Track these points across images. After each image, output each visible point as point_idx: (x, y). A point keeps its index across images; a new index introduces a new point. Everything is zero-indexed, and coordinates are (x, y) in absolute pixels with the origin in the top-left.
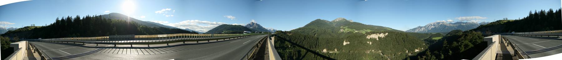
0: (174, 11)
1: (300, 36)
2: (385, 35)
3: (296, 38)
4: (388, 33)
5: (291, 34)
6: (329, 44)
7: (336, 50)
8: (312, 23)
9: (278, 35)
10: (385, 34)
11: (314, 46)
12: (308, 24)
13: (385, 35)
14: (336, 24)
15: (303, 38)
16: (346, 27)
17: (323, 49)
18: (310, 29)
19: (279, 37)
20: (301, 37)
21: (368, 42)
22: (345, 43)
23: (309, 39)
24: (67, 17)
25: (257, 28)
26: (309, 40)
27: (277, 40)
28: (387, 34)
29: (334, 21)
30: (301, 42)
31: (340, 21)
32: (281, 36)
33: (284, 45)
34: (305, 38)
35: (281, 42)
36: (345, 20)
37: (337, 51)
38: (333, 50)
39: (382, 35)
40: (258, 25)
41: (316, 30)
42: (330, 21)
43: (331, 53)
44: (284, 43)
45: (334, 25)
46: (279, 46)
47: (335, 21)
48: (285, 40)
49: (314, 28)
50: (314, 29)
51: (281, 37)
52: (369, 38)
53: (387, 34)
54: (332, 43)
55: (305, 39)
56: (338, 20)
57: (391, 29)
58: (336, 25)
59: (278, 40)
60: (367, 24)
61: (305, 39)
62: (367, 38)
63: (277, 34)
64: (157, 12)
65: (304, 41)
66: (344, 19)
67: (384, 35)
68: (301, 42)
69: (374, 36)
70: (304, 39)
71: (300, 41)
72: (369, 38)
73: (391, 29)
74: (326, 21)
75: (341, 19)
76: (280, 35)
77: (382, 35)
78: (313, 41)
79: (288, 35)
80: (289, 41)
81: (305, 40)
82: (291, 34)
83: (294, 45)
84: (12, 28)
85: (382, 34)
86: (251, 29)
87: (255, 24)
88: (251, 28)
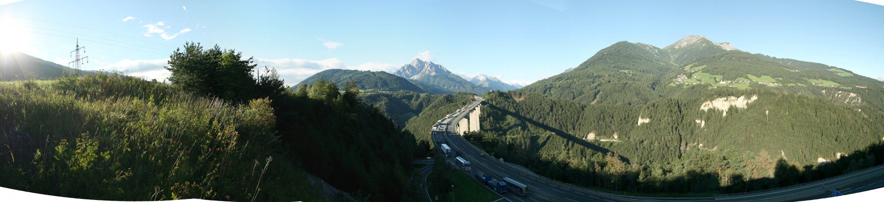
0: (184, 8)
1: (541, 104)
2: (749, 101)
3: (531, 109)
4: (759, 94)
5: (522, 99)
6: (603, 123)
7: (616, 137)
8: (601, 57)
9: (490, 102)
10: (749, 99)
11: (570, 127)
12: (585, 63)
13: (749, 101)
14: (677, 56)
15: (547, 109)
16: (700, 68)
17: (588, 133)
18: (588, 77)
19: (492, 106)
20: (543, 105)
21: (698, 121)
22: (640, 121)
23: (563, 110)
24: (212, 47)
25: (435, 77)
26: (560, 112)
27: (486, 115)
28: (755, 98)
29: (672, 48)
30: (541, 117)
31: (692, 45)
32: (497, 104)
33: (502, 126)
34: (552, 107)
35: (494, 120)
36: (708, 42)
37: (619, 137)
38: (610, 136)
39: (741, 103)
40: (438, 69)
41: (607, 78)
42: (661, 47)
43: (602, 142)
44: (504, 119)
45: (672, 62)
46: (490, 128)
47: (677, 47)
48: (506, 112)
49: (600, 74)
50: (599, 77)
51: (497, 106)
52: (706, 109)
53: (755, 98)
54: (610, 118)
55: (552, 110)
56: (684, 44)
57: (849, 74)
58: (676, 61)
59: (488, 116)
60: (779, 56)
61: (552, 110)
62: (702, 108)
63: (488, 100)
64: (125, 20)
65: (548, 114)
66: (705, 41)
67: (745, 102)
68: (541, 117)
69: (721, 105)
70: (548, 110)
71: (539, 116)
72: (706, 109)
73: (851, 72)
74: (647, 46)
75: (694, 40)
76: (494, 103)
77: (741, 103)
78: (571, 114)
79: (514, 102)
80: (516, 115)
81: (551, 113)
82: (522, 99)
83: (523, 122)
84: (323, 78)
85: (742, 98)
86: (416, 81)
87: (426, 66)
88: (415, 77)
